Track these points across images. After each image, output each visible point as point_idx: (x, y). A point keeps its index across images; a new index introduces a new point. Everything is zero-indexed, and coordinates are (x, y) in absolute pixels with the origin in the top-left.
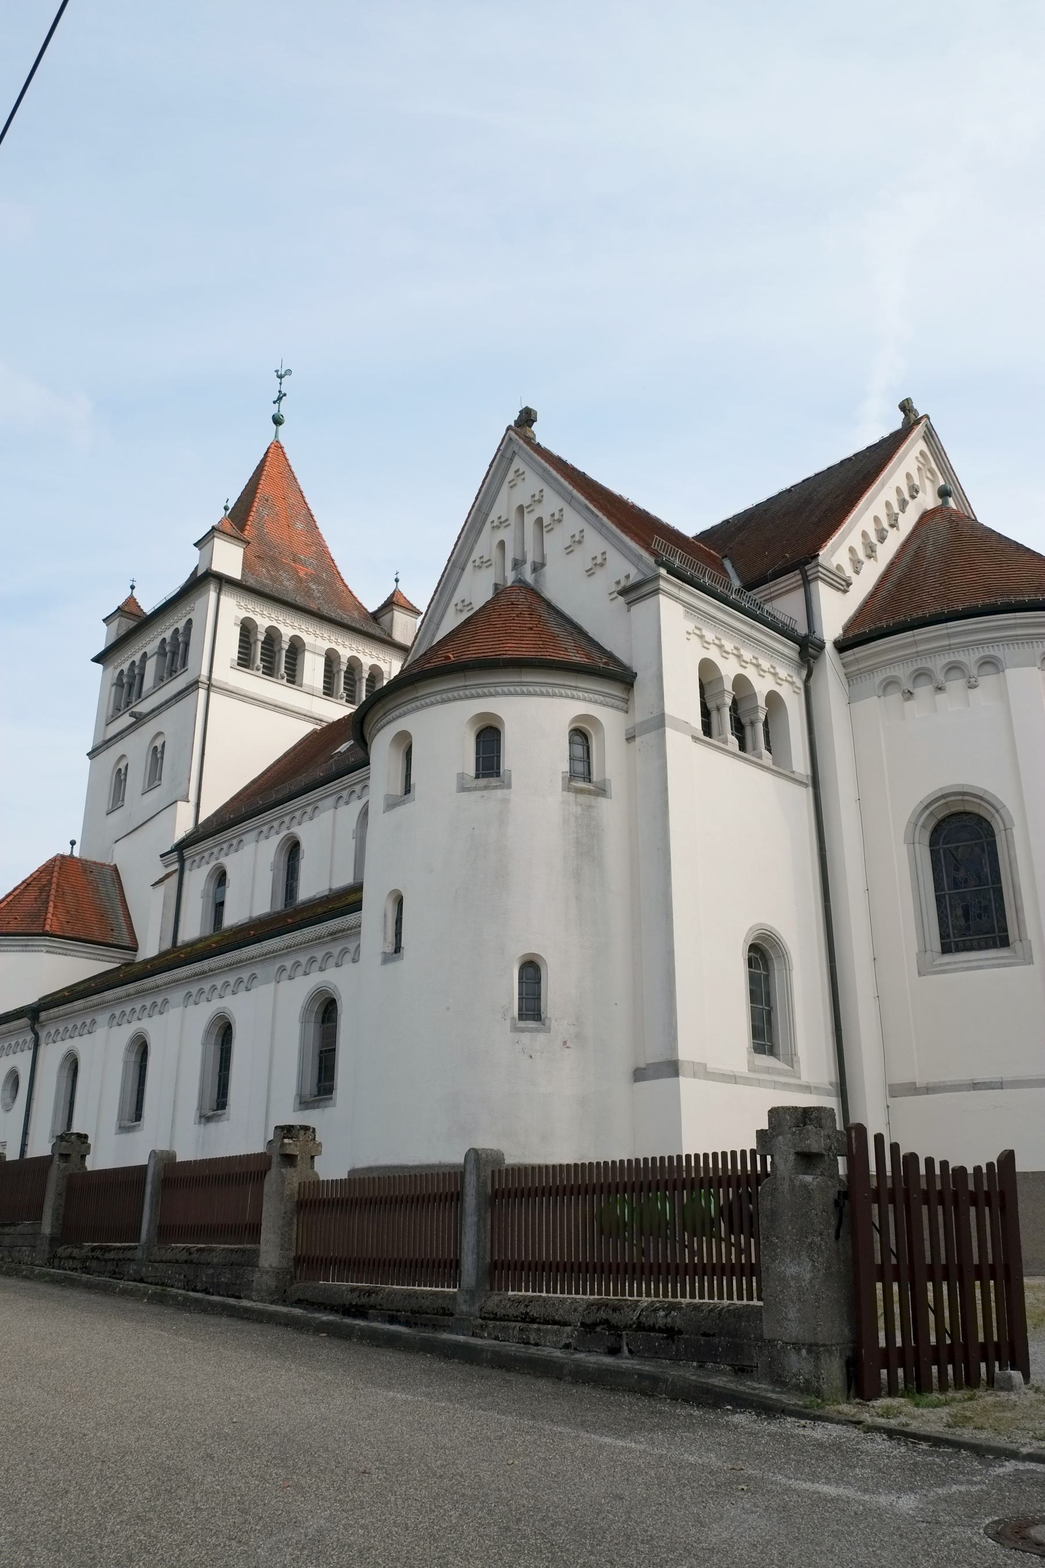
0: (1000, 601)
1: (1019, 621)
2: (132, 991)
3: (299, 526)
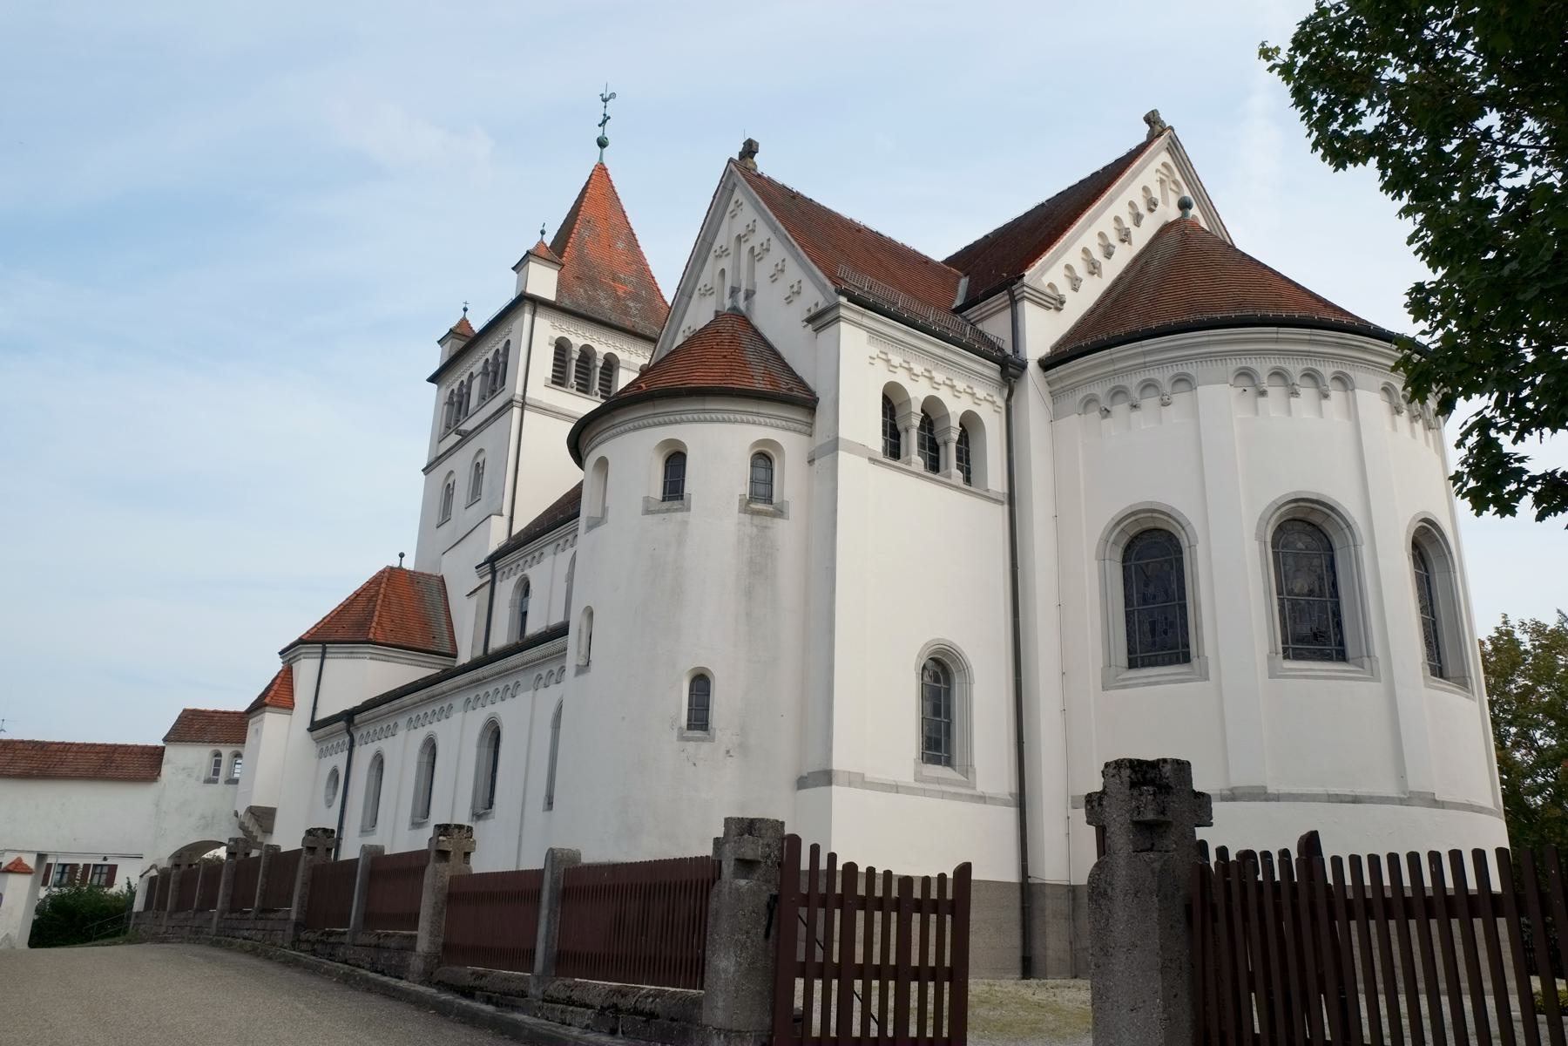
0: (1205, 317)
1: (1212, 338)
2: (424, 696)
3: (620, 245)
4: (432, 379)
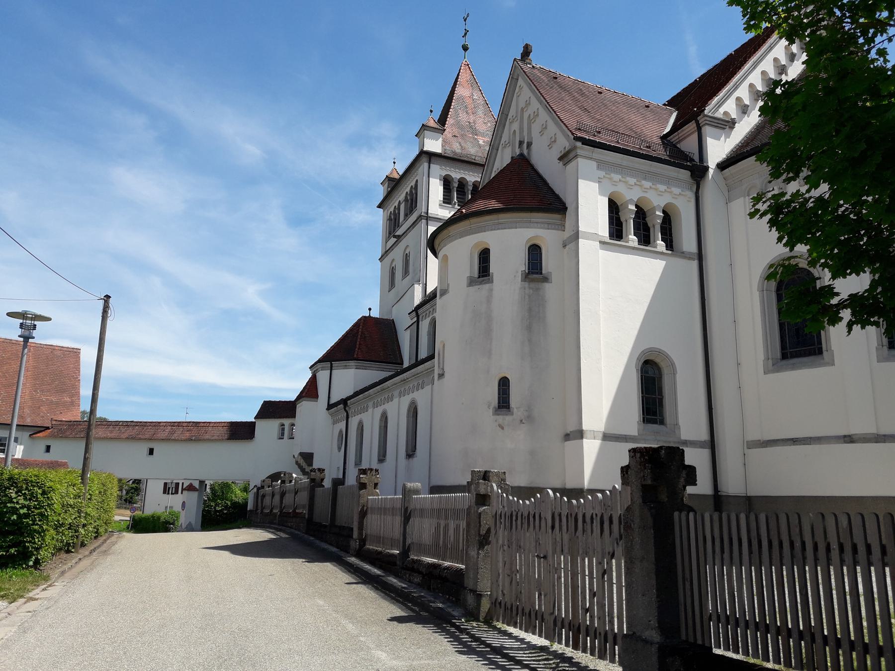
4: (379, 206)
